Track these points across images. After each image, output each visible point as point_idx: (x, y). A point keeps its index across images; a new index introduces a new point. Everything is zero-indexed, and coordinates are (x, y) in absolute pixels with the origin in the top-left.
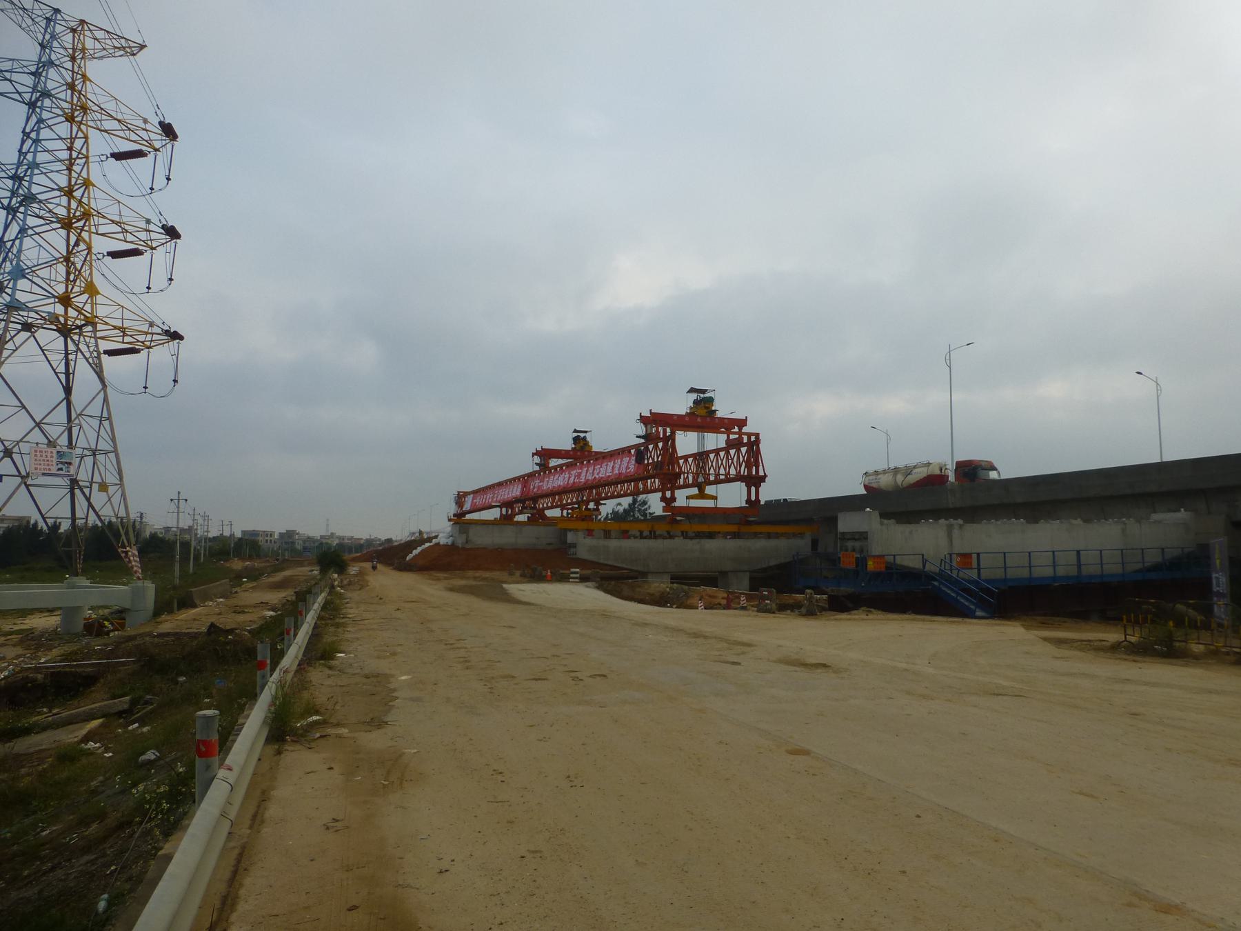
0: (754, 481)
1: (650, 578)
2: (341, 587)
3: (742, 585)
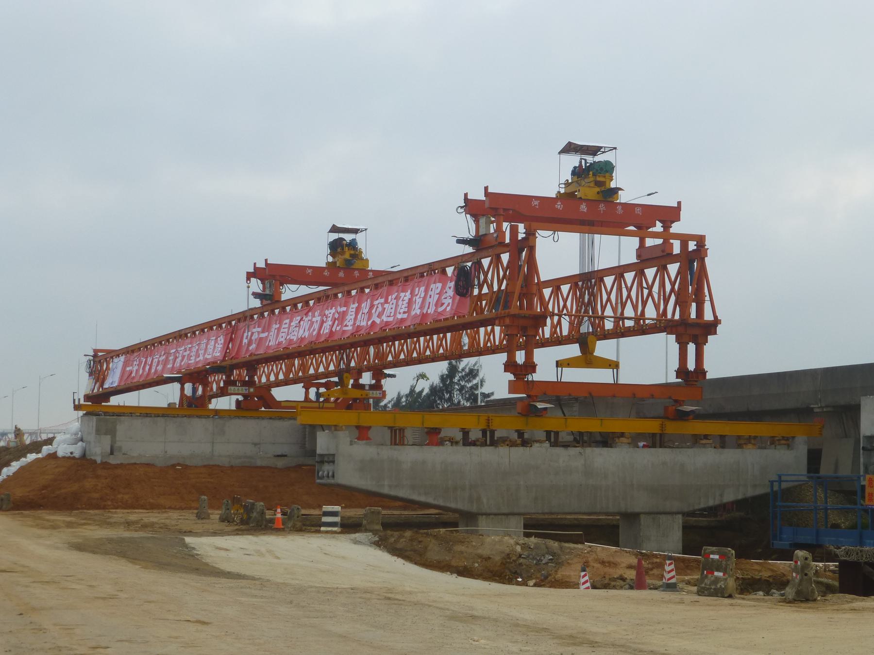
0: (695, 331)
1: (483, 525)
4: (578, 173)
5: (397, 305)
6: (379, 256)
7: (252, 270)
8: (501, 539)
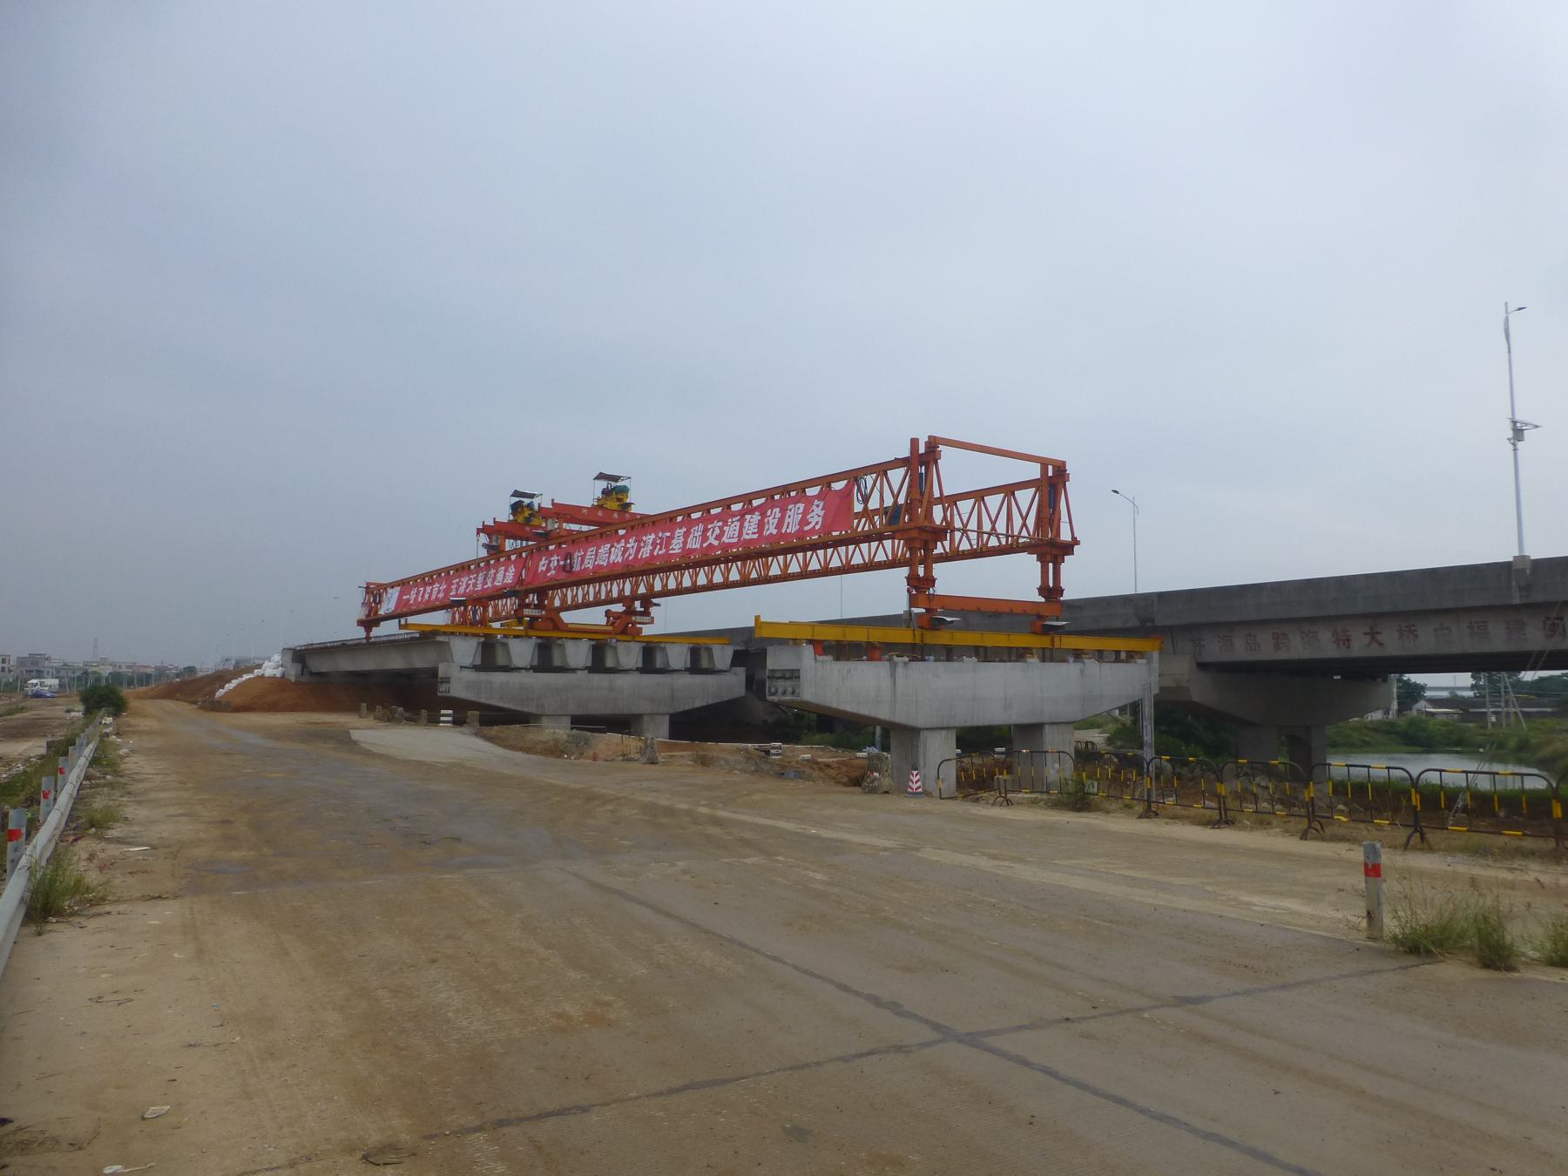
0: (1052, 550)
1: (545, 722)
2: (118, 734)
3: (658, 731)
4: (606, 492)
5: (741, 527)
6: (643, 503)
7: (505, 516)
8: (559, 731)
